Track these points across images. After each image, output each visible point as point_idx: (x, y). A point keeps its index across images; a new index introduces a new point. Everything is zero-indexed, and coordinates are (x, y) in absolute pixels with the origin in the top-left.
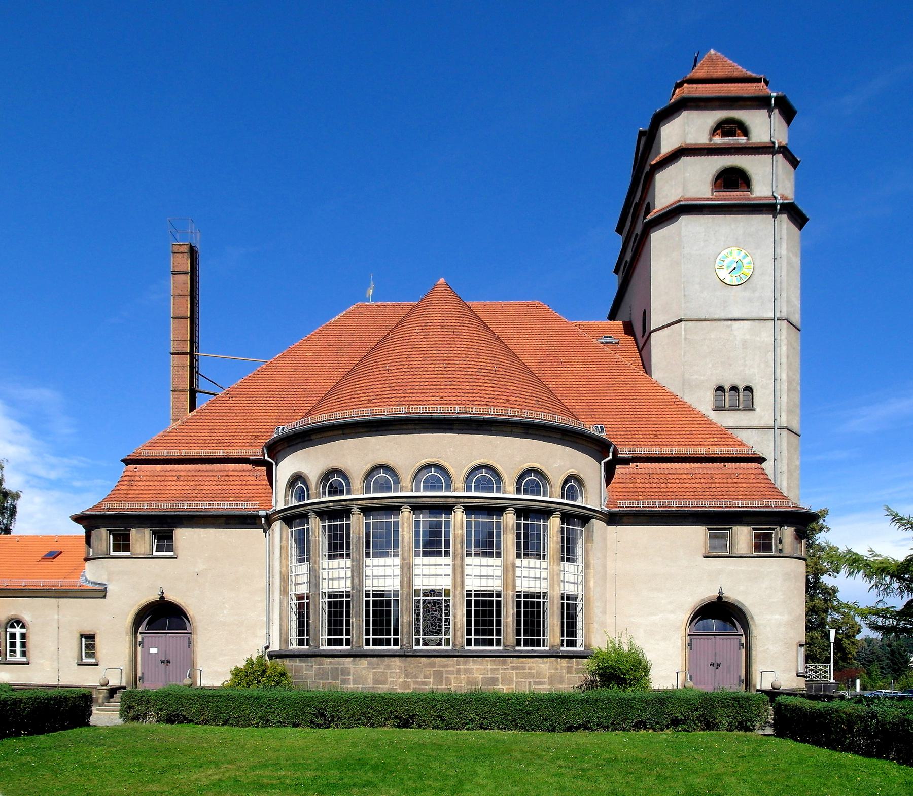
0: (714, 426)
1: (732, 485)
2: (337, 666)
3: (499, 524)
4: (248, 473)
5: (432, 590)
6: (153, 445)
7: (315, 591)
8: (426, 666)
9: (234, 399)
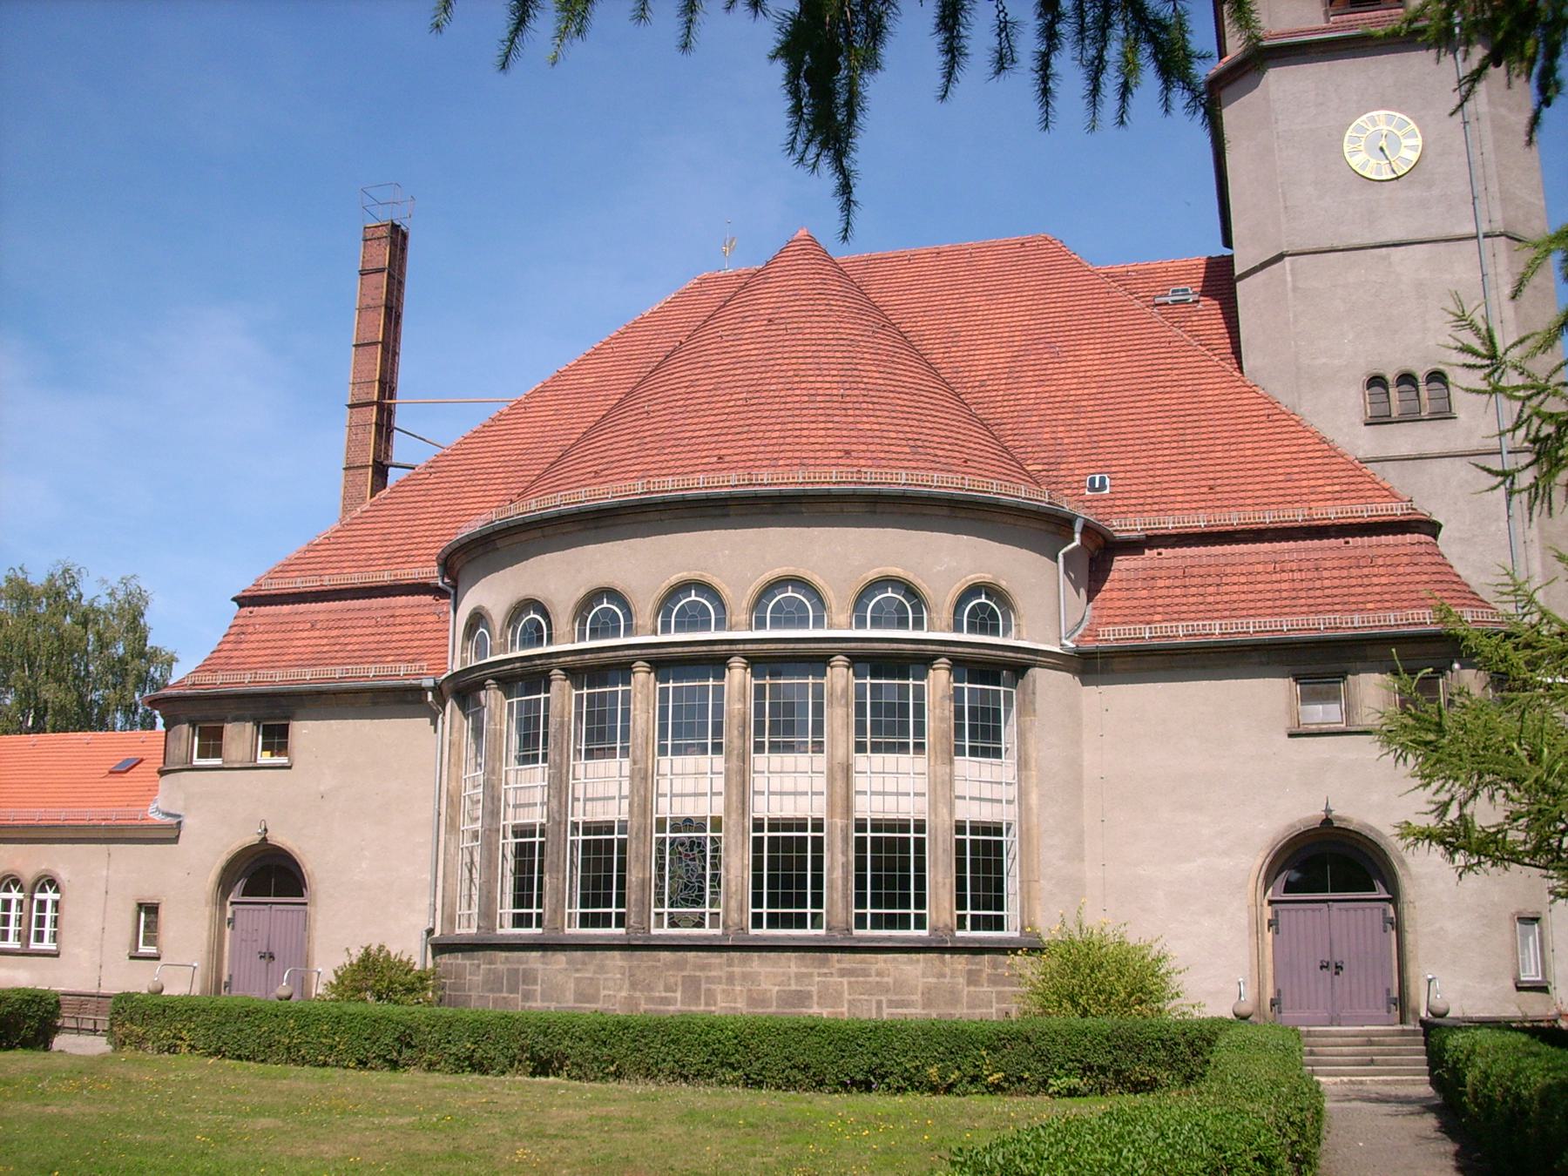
0: (1341, 460)
1: (1359, 581)
2: (516, 966)
3: (819, 691)
4: (427, 610)
5: (688, 820)
6: (285, 569)
7: (491, 825)
8: (668, 966)
9: (438, 475)
